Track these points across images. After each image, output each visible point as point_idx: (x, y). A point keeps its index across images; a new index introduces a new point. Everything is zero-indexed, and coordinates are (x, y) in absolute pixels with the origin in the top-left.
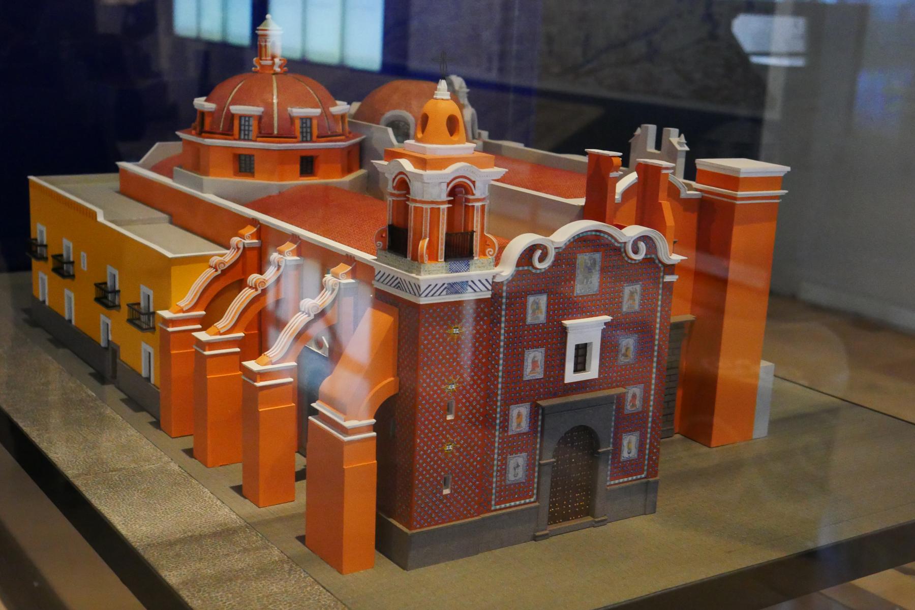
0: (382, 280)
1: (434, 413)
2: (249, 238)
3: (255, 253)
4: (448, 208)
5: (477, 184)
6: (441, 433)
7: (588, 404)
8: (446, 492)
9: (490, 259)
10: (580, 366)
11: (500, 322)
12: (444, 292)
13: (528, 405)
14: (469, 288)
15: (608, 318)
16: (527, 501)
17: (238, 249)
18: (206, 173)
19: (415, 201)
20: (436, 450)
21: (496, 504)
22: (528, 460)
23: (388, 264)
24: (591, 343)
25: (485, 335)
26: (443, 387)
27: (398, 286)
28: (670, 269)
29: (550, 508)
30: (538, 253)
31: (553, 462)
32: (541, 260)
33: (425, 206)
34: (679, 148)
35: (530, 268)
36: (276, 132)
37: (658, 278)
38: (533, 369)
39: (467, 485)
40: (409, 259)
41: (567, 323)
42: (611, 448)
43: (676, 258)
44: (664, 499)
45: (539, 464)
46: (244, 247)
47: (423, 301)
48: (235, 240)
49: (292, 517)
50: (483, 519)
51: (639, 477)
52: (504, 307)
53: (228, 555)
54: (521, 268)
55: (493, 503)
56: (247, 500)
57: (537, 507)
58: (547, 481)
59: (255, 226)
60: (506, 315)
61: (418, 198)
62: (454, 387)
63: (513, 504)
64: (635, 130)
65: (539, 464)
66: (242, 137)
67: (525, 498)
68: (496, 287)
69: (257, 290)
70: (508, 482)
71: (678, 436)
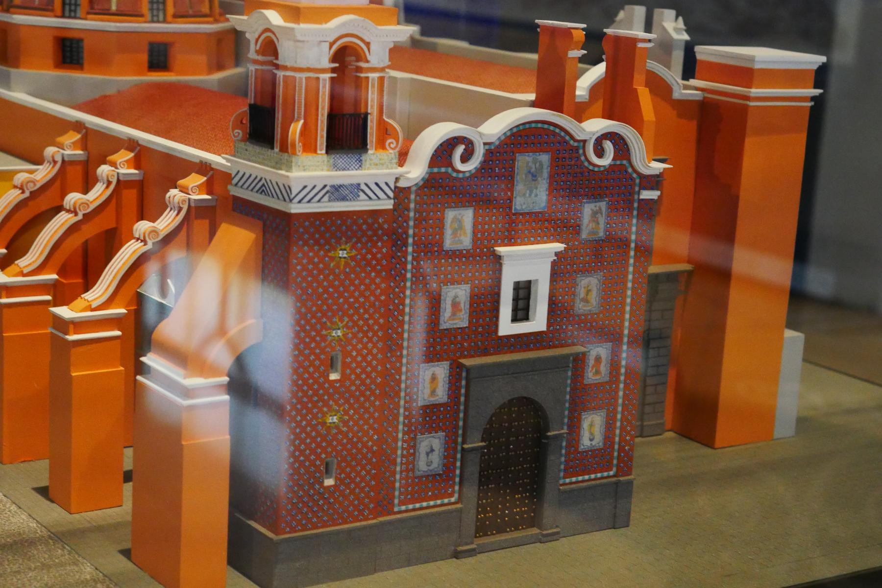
0: (240, 184)
1: (311, 370)
2: (70, 147)
3: (79, 168)
4: (332, 79)
5: (373, 47)
6: (321, 399)
7: (532, 366)
8: (329, 482)
9: (391, 153)
10: (521, 312)
11: (406, 244)
12: (326, 198)
13: (446, 365)
14: (361, 194)
15: (560, 247)
16: (446, 501)
17: (55, 162)
18: (16, 64)
19: (285, 68)
20: (314, 422)
21: (401, 503)
22: (446, 443)
23: (249, 161)
24: (537, 280)
25: (384, 262)
26: (324, 332)
27: (263, 190)
28: (652, 181)
29: (478, 513)
30: (460, 149)
31: (482, 448)
32: (465, 159)
33: (298, 75)
34: (675, 36)
35: (450, 170)
36: (114, 8)
37: (631, 194)
38: (454, 314)
39: (358, 474)
40: (277, 150)
41: (501, 250)
42: (565, 430)
43: (657, 167)
44: (644, 510)
45: (463, 449)
46: (63, 161)
47: (295, 208)
48: (50, 151)
49: (117, 526)
50: (383, 524)
51: (605, 474)
52: (411, 223)
53: (18, 572)
54: (436, 170)
55: (396, 501)
56: (55, 505)
57: (460, 511)
58: (473, 470)
59: (79, 132)
60: (415, 235)
61: (288, 64)
62: (339, 333)
63: (425, 504)
64: (616, 15)
65: (463, 449)
66: (67, 14)
67: (442, 498)
68: (401, 193)
69: (76, 214)
70: (418, 473)
71: (670, 434)
